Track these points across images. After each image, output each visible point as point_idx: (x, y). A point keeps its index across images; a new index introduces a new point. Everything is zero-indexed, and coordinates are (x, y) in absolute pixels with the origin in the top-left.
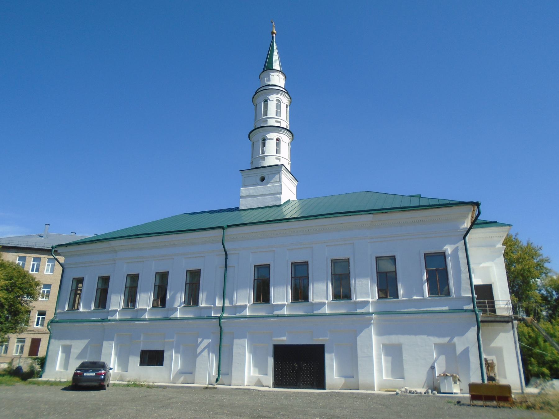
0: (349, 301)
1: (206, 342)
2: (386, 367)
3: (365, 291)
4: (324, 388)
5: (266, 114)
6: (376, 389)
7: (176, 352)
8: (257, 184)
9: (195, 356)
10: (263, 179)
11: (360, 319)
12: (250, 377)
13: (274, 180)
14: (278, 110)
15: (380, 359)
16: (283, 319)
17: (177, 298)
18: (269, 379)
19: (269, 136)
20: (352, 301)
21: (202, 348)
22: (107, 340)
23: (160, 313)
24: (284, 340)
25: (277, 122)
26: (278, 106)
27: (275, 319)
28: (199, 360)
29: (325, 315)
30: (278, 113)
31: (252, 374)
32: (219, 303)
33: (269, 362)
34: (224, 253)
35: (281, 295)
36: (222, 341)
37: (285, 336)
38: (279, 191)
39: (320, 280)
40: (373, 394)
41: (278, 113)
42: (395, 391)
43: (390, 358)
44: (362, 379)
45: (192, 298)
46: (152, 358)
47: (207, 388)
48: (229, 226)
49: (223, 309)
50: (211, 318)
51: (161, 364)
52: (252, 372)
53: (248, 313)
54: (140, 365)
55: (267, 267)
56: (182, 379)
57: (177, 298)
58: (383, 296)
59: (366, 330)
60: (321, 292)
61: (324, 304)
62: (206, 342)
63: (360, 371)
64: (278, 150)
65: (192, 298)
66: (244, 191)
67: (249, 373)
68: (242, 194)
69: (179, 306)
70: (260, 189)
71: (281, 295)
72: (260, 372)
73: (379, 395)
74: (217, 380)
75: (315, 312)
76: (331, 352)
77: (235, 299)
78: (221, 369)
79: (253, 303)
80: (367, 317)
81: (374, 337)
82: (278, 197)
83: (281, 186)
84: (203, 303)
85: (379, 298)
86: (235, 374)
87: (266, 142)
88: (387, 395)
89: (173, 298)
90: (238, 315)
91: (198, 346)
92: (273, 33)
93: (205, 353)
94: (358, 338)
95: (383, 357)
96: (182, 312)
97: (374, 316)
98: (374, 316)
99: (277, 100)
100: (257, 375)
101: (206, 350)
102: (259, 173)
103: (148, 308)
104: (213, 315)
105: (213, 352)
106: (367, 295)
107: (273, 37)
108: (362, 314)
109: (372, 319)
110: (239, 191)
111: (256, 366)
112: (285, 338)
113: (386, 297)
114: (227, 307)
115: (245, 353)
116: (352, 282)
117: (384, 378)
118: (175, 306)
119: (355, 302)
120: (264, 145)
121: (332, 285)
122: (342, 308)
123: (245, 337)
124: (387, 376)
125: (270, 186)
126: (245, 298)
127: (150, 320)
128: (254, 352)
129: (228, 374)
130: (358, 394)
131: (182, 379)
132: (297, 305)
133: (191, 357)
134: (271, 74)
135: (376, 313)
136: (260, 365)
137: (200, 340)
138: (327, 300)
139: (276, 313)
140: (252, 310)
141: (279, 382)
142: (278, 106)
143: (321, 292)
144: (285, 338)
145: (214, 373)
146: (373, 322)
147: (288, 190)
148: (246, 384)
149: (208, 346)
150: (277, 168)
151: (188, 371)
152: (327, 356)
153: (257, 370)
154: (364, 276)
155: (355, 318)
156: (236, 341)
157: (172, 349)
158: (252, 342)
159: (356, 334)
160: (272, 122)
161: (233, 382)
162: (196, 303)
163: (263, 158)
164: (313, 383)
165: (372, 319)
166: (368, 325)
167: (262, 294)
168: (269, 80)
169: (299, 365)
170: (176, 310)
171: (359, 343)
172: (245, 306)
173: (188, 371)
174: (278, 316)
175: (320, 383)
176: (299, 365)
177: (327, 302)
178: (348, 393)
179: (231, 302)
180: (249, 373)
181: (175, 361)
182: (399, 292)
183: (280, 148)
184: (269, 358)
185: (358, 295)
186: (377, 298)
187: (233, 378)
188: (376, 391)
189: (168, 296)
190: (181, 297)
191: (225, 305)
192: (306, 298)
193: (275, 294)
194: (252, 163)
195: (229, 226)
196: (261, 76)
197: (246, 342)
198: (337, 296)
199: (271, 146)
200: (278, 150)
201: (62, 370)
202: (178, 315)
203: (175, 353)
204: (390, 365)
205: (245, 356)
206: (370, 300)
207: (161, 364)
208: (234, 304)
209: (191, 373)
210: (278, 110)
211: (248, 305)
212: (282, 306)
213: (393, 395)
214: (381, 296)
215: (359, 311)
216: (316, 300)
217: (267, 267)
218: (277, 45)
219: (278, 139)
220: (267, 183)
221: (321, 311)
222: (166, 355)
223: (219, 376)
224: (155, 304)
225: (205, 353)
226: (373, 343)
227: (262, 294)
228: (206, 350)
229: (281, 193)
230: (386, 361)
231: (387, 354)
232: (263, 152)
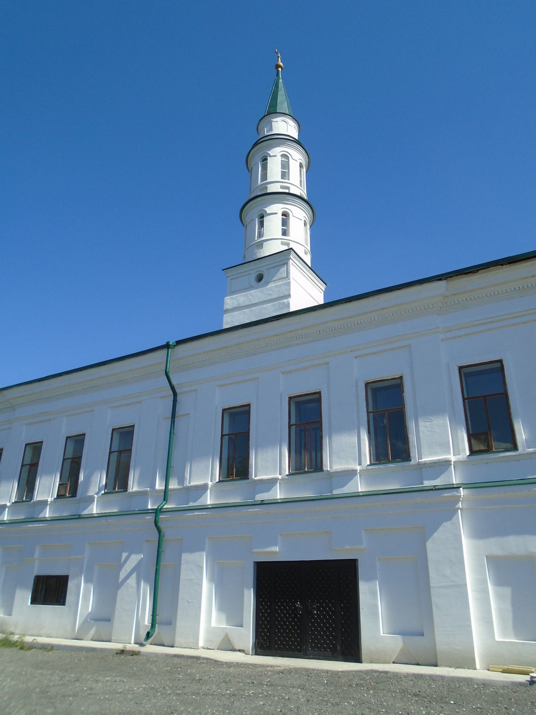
0: (406, 464)
1: (135, 559)
2: (500, 611)
3: (441, 440)
4: (357, 659)
5: (265, 176)
6: (478, 666)
7: (87, 581)
8: (251, 288)
9: (117, 585)
10: (260, 278)
11: (432, 501)
12: (210, 631)
13: (279, 275)
14: (287, 168)
15: (483, 592)
16: (273, 509)
17: (95, 480)
18: (247, 636)
19: (268, 210)
20: (412, 462)
21: (129, 570)
22: (193, 549)
23: (68, 508)
24: (276, 552)
25: (282, 187)
26: (285, 166)
27: (256, 509)
28: (122, 593)
29: (356, 496)
30: (285, 175)
31: (214, 624)
32: (159, 485)
33: (246, 599)
34: (171, 392)
35: (270, 463)
36: (162, 556)
37: (276, 545)
38: (286, 293)
39: (346, 427)
40: (468, 681)
41: (285, 175)
42: (527, 673)
43: (507, 591)
44: (443, 639)
45: (119, 480)
46: (50, 590)
47: (123, 652)
48: (179, 343)
49: (166, 494)
50: (146, 512)
51: (63, 603)
52: (214, 622)
53: (209, 500)
54: (32, 603)
55: (497, 368)
56: (92, 632)
57: (95, 480)
58: (482, 447)
59: (447, 525)
60: (348, 450)
61: (351, 473)
62: (135, 559)
63: (436, 620)
64: (286, 229)
65: (119, 480)
66: (229, 302)
67: (209, 621)
68: (226, 307)
69: (97, 494)
70: (256, 294)
71: (270, 463)
72: (229, 621)
73: (485, 684)
74: (148, 635)
75: (336, 492)
76: (371, 578)
77: (188, 476)
78: (158, 612)
79: (220, 481)
80: (447, 494)
81: (466, 543)
82: (284, 303)
83: (289, 283)
84: (133, 487)
85: (472, 452)
86: (181, 623)
87: (265, 219)
88: (505, 686)
89: (88, 479)
90: (191, 504)
91: (121, 566)
92: (278, 66)
93: (132, 581)
94: (429, 545)
95: (490, 588)
96: (101, 504)
97: (462, 492)
98: (462, 492)
99: (283, 156)
100: (224, 626)
101: (134, 575)
102: (253, 270)
103: (49, 500)
104: (149, 507)
105: (146, 581)
106: (445, 447)
107: (278, 71)
108: (435, 489)
109: (457, 499)
110: (222, 303)
111: (221, 608)
112: (276, 549)
113: (488, 450)
114: (174, 490)
115: (201, 580)
116: (411, 425)
117: (498, 638)
118: (90, 494)
119: (419, 464)
120: (262, 224)
121: (369, 433)
122: (392, 477)
123: (203, 549)
124: (504, 633)
125: (271, 288)
126: (205, 474)
127: (53, 520)
128: (220, 580)
129: (170, 623)
130: (433, 678)
131: (92, 632)
132: (300, 478)
133: (109, 588)
134: (274, 120)
135: (467, 486)
136: (229, 606)
137: (124, 555)
138: (360, 464)
139: (259, 497)
140: (217, 493)
141: (265, 644)
142: (285, 166)
143: (348, 450)
144: (276, 549)
145: (147, 621)
146: (460, 505)
147: (304, 290)
148: (201, 644)
149: (136, 569)
150: (283, 257)
151: (103, 618)
152: (363, 588)
153: (224, 617)
154: (435, 411)
155: (418, 498)
156: (185, 557)
157: (81, 574)
158: (215, 558)
159: (424, 536)
160: (272, 188)
161: (179, 639)
162: (124, 486)
163: (260, 245)
164: (335, 646)
165: (457, 499)
166: (450, 513)
167: (236, 466)
168: (271, 129)
169: (306, 604)
170: (91, 500)
171: (431, 555)
172: (204, 487)
173: (103, 618)
174: (262, 503)
175: (348, 646)
176: (306, 604)
177: (358, 468)
178: (407, 676)
179: (181, 480)
180: (209, 621)
181: (83, 596)
182: (518, 437)
183: (288, 228)
184: (246, 592)
185: (424, 451)
186: (468, 453)
187: (178, 630)
188: (479, 673)
189: (81, 478)
190: (100, 479)
191: (171, 486)
192: (317, 466)
193: (259, 461)
194: (244, 257)
195: (179, 343)
196: (260, 127)
197: (203, 558)
198: (380, 456)
199: (273, 225)
200: (286, 229)
201: (224, 626)
202: (95, 509)
203: (86, 581)
204: (509, 607)
205: (200, 585)
206: (453, 458)
207: (63, 603)
208: (187, 484)
209: (170, 623)
210: (287, 168)
211: (210, 483)
212: (273, 482)
213: (521, 684)
214: (476, 448)
215: (427, 483)
216: (338, 467)
217: (497, 368)
218: (284, 82)
219: (285, 215)
220: (267, 283)
221: (347, 489)
222: (71, 585)
223: (153, 626)
224: (62, 493)
225: (132, 581)
226: (466, 556)
227: (236, 466)
228: (134, 575)
229: (289, 296)
230: (499, 597)
231: (499, 582)
232: (260, 235)
